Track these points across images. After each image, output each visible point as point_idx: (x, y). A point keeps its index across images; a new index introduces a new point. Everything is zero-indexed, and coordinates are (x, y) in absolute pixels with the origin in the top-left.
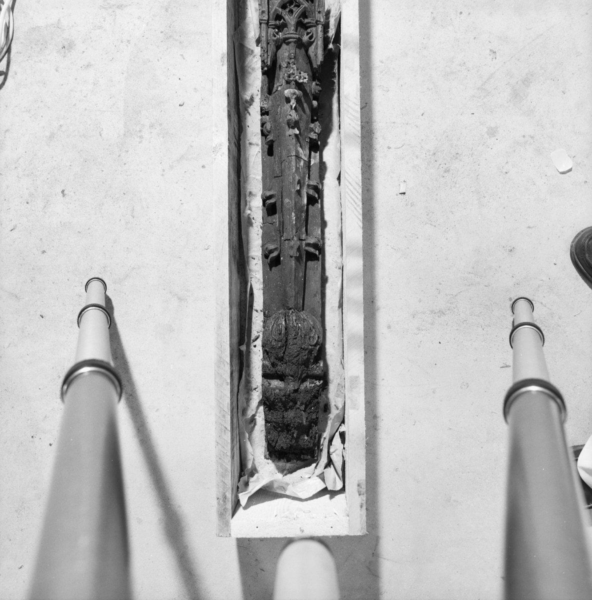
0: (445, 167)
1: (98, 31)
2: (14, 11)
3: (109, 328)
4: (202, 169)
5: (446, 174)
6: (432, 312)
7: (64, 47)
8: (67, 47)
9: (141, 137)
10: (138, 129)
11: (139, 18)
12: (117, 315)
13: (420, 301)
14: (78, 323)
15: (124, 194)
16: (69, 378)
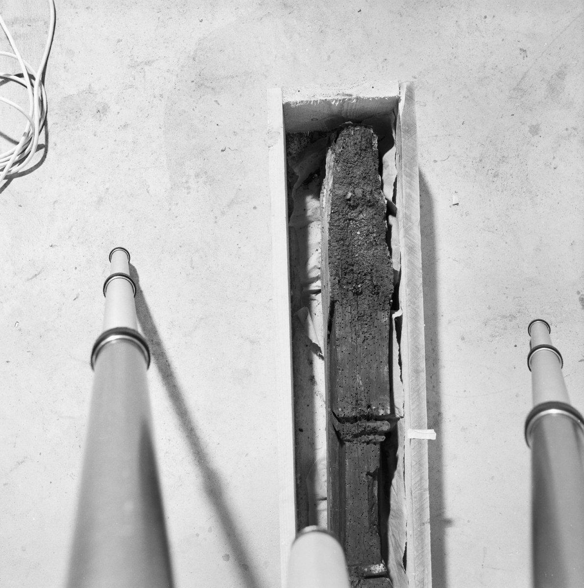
0: (493, 172)
1: (130, 89)
2: (45, 83)
3: (135, 296)
4: (254, 211)
5: (495, 179)
6: (504, 317)
7: (99, 111)
8: (102, 111)
9: (188, 188)
10: (184, 181)
11: (168, 71)
12: (143, 283)
13: (489, 308)
14: (104, 293)
15: (180, 246)
16: (97, 349)
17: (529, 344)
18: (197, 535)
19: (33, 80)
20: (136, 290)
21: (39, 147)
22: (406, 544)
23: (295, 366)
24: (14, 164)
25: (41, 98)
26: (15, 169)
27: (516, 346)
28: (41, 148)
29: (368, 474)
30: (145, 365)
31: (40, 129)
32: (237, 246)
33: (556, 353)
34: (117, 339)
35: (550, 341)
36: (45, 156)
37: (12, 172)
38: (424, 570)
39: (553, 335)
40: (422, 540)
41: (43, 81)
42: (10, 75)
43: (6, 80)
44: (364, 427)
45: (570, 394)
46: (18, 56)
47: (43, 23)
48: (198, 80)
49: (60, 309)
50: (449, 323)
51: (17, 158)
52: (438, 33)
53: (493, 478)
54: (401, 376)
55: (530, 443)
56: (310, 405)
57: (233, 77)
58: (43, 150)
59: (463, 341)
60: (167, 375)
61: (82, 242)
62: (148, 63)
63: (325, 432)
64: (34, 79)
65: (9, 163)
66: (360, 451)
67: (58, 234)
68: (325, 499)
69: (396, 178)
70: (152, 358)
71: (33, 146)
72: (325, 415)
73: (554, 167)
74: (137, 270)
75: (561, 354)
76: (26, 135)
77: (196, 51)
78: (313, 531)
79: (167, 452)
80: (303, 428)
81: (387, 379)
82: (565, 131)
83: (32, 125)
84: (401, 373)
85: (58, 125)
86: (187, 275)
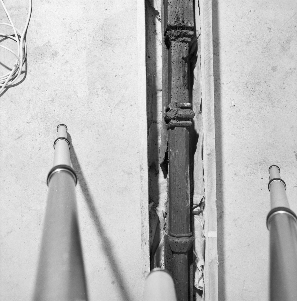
3: (69, 149)
5: (253, 94)
6: (257, 164)
7: (53, 54)
8: (54, 54)
9: (98, 95)
10: (96, 91)
15: (93, 124)
16: (50, 176)
17: (269, 178)
18: (99, 271)
19: (20, 38)
20: (70, 146)
21: (22, 72)
22: (202, 99)
23: (147, 52)
24: (9, 81)
25: (24, 47)
26: (10, 83)
27: (262, 178)
28: (23, 73)
29: (183, 58)
30: (74, 184)
31: (23, 63)
32: (122, 125)
33: (283, 182)
34: (60, 171)
35: (280, 176)
36: (25, 77)
37: (8, 85)
38: (210, 99)
39: (281, 173)
40: (210, 84)
41: (25, 39)
42: (9, 35)
43: (6, 37)
44: (181, 32)
45: (290, 204)
46: (13, 25)
47: (25, 9)
48: (103, 40)
49: (31, 155)
50: (229, 166)
51: (11, 78)
52: (226, 19)
53: (249, 245)
54: (199, 12)
55: (269, 228)
56: (154, 45)
57: (121, 39)
58: (24, 74)
59: (236, 175)
60: (85, 190)
61: (43, 121)
62: (78, 31)
63: (161, 58)
64: (21, 37)
65: (7, 80)
66: (179, 46)
67: (31, 116)
68: (161, 91)
69: (204, 189)
70: (78, 182)
71: (19, 72)
72: (162, 50)
73: (284, 88)
74: (71, 136)
75: (285, 183)
76: (16, 66)
77: (103, 25)
78: (158, 270)
79: (84, 229)
80: (150, 56)
81: (192, 9)
82: (290, 70)
83: (19, 61)
84: (200, 11)
85: (32, 61)
86: (96, 139)
